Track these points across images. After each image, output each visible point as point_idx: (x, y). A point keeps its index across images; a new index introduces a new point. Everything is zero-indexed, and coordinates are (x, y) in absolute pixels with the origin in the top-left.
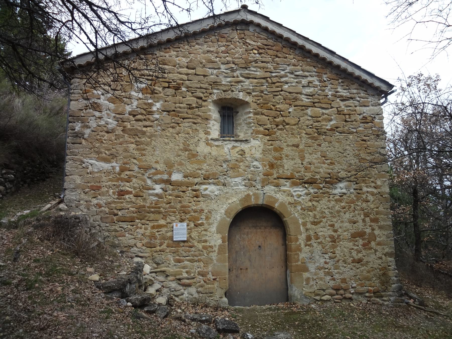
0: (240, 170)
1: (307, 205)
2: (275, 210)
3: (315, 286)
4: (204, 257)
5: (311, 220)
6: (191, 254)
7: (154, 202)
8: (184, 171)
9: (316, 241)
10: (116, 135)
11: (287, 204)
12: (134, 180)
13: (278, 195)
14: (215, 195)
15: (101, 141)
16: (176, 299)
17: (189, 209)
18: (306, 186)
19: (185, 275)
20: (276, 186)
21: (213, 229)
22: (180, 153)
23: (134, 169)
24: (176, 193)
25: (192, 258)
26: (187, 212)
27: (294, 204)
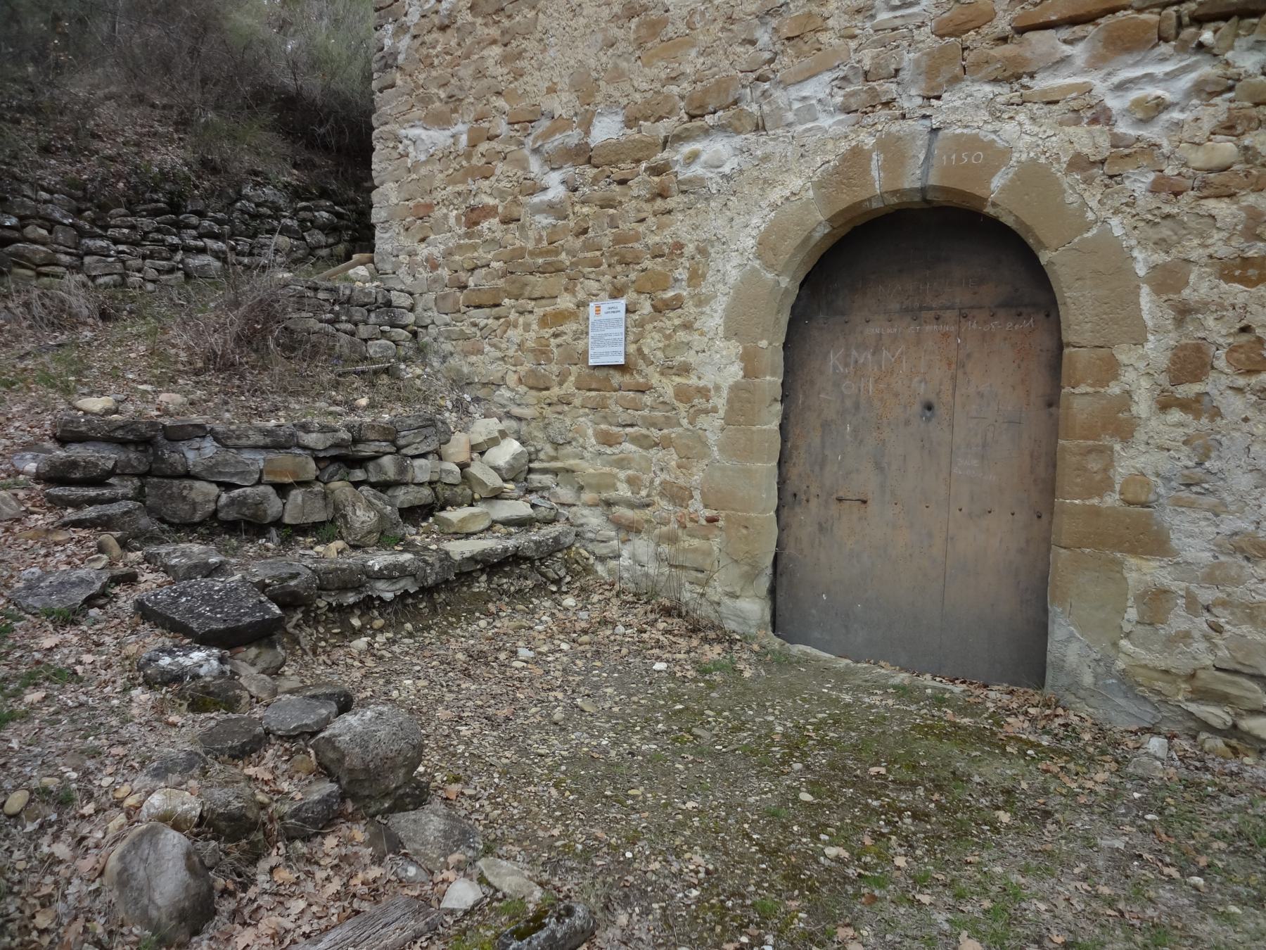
0: (824, 37)
1: (1198, 158)
2: (989, 210)
3: (1202, 645)
4: (680, 430)
5: (1222, 251)
6: (643, 417)
7: (544, 234)
8: (624, 101)
9: (1241, 382)
10: (458, 29)
11: (1058, 169)
12: (500, 167)
13: (1009, 129)
14: (724, 176)
15: (429, 61)
16: (600, 568)
17: (636, 245)
18: (1207, 36)
19: (624, 491)
20: (1007, 80)
21: (714, 320)
22: (615, 32)
23: (498, 132)
24: (601, 190)
25: (644, 431)
26: (629, 258)
27: (1103, 168)
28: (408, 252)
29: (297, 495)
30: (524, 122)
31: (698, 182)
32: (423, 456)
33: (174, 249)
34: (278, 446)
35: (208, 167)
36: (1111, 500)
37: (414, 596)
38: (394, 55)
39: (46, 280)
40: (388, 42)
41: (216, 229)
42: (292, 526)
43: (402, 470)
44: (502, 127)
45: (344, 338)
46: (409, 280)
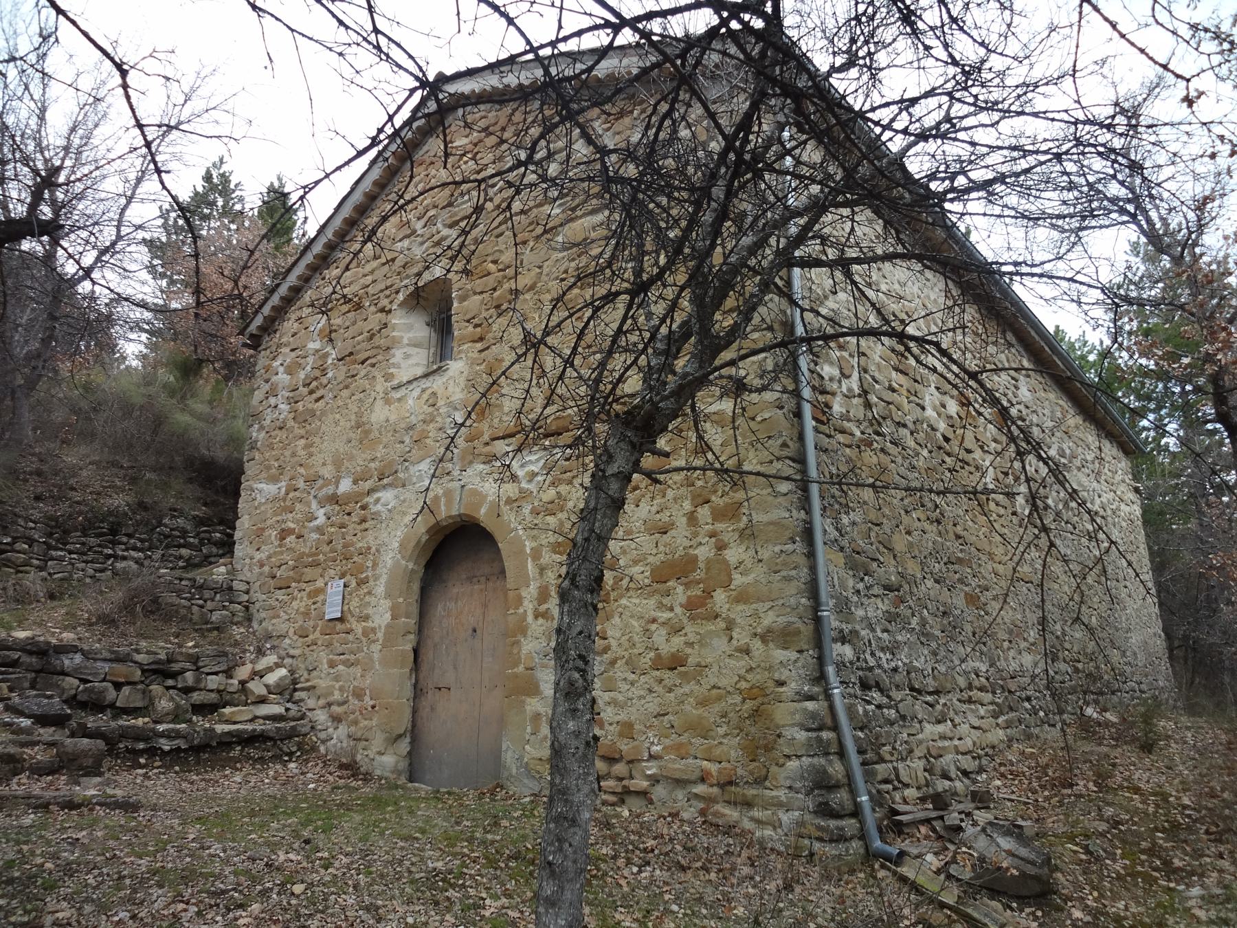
0: (428, 441)
12: (298, 506)
19: (337, 696)
21: (380, 589)
28: (252, 556)
29: (126, 690)
30: (310, 481)
31: (378, 513)
32: (216, 673)
33: (108, 557)
34: (118, 660)
35: (142, 506)
36: (521, 668)
37: (185, 751)
38: (256, 442)
39: (20, 575)
40: (254, 434)
41: (139, 544)
42: (121, 708)
43: (198, 680)
44: (301, 484)
45: (195, 609)
46: (249, 574)
